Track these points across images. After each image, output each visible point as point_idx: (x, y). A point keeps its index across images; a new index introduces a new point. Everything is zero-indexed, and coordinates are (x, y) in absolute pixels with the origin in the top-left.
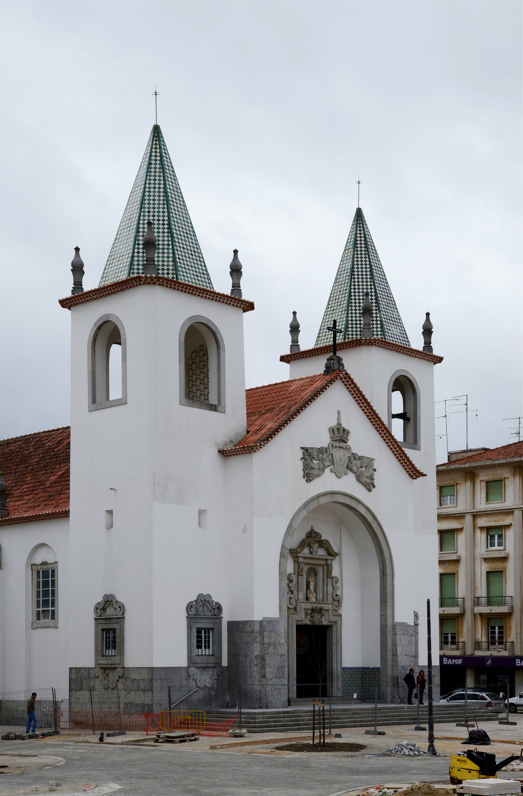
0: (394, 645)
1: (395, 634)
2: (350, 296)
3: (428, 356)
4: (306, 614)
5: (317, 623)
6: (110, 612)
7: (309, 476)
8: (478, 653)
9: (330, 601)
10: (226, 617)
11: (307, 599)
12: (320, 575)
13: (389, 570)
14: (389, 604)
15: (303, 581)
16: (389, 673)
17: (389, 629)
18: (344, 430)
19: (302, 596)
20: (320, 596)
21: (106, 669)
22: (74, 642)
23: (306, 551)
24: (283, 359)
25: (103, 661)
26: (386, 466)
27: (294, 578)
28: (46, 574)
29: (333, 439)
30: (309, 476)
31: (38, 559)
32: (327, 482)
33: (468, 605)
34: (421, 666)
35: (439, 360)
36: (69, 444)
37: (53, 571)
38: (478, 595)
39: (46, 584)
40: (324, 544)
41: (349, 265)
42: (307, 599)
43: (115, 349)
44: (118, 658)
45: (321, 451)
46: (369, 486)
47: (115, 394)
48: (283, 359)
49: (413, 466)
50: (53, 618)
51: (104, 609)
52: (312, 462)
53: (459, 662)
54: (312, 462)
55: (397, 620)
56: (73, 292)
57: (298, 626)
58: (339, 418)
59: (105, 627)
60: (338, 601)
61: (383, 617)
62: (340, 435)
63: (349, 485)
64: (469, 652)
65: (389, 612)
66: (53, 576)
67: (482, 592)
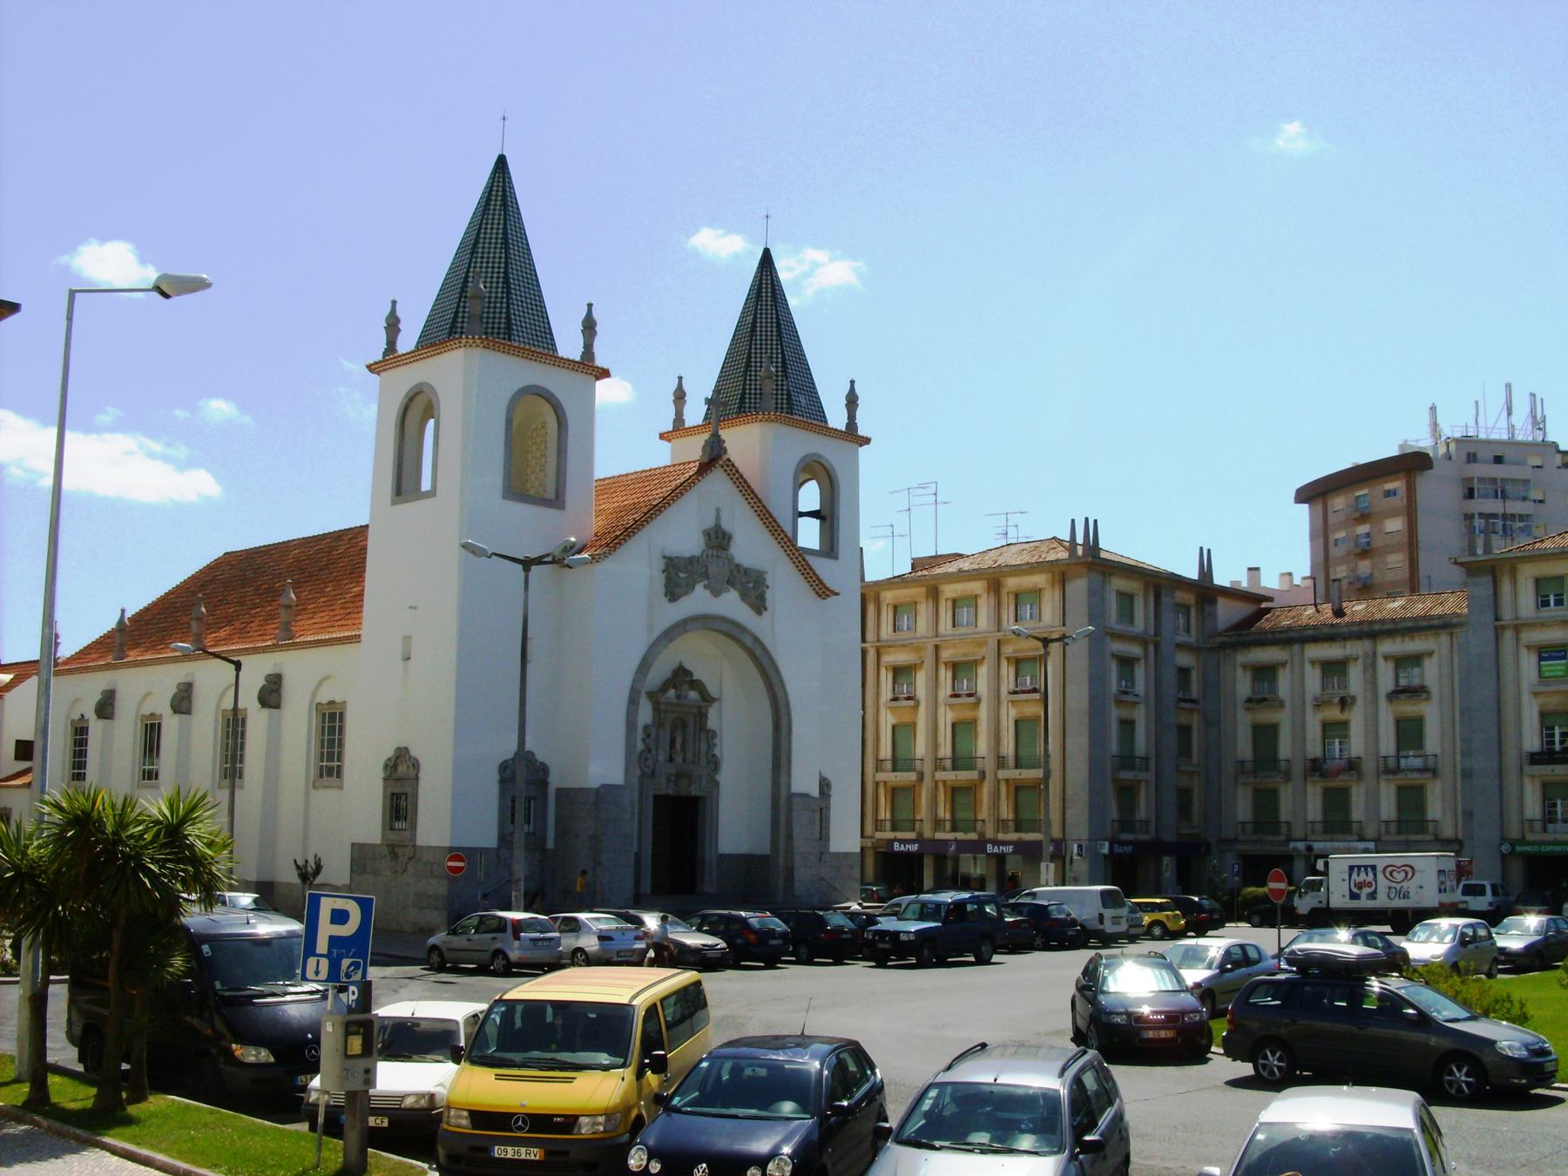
0: (789, 821)
1: (790, 810)
2: (749, 357)
3: (852, 436)
4: (669, 780)
5: (683, 793)
6: (402, 769)
7: (673, 592)
8: (940, 835)
9: (703, 761)
10: (555, 782)
11: (671, 760)
12: (691, 729)
13: (784, 722)
14: (784, 768)
15: (665, 735)
16: (781, 861)
17: (782, 802)
18: (724, 534)
19: (662, 757)
20: (690, 756)
21: (393, 850)
22: (357, 811)
23: (672, 693)
24: (662, 436)
25: (392, 836)
26: (783, 583)
27: (653, 732)
28: (332, 716)
29: (709, 545)
30: (673, 592)
31: (324, 698)
32: (699, 600)
33: (928, 769)
34: (838, 854)
35: (867, 441)
36: (364, 549)
37: (341, 714)
38: (941, 754)
39: (332, 730)
40: (697, 685)
41: (750, 319)
42: (671, 760)
43: (431, 422)
44: (407, 834)
45: (692, 560)
46: (759, 606)
47: (426, 485)
48: (662, 436)
49: (821, 582)
50: (339, 775)
51: (395, 767)
52: (678, 576)
53: (914, 848)
54: (678, 576)
55: (795, 788)
56: (385, 354)
57: (656, 797)
58: (718, 517)
59: (396, 790)
60: (715, 764)
61: (776, 784)
62: (718, 539)
63: (731, 605)
64: (928, 834)
65: (783, 780)
66: (341, 720)
67: (945, 750)
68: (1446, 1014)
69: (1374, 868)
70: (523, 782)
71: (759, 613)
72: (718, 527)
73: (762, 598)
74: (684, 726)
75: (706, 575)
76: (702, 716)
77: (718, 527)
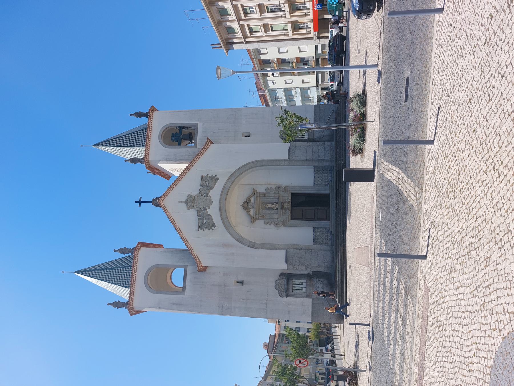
7: (211, 226)
12: (265, 200)
30: (211, 226)
32: (213, 211)
46: (215, 179)
58: (182, 202)
60: (279, 188)
62: (190, 202)
63: (215, 194)
68: (410, 318)
69: (268, 12)
70: (286, 282)
71: (218, 179)
72: (186, 202)
73: (212, 178)
74: (265, 203)
75: (205, 209)
76: (261, 195)
77: (186, 202)
